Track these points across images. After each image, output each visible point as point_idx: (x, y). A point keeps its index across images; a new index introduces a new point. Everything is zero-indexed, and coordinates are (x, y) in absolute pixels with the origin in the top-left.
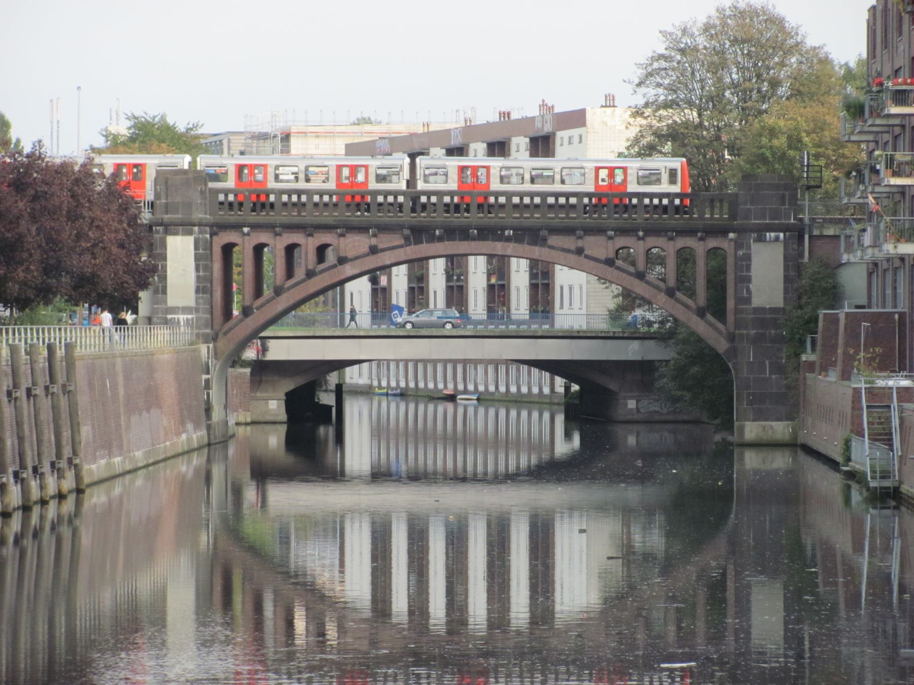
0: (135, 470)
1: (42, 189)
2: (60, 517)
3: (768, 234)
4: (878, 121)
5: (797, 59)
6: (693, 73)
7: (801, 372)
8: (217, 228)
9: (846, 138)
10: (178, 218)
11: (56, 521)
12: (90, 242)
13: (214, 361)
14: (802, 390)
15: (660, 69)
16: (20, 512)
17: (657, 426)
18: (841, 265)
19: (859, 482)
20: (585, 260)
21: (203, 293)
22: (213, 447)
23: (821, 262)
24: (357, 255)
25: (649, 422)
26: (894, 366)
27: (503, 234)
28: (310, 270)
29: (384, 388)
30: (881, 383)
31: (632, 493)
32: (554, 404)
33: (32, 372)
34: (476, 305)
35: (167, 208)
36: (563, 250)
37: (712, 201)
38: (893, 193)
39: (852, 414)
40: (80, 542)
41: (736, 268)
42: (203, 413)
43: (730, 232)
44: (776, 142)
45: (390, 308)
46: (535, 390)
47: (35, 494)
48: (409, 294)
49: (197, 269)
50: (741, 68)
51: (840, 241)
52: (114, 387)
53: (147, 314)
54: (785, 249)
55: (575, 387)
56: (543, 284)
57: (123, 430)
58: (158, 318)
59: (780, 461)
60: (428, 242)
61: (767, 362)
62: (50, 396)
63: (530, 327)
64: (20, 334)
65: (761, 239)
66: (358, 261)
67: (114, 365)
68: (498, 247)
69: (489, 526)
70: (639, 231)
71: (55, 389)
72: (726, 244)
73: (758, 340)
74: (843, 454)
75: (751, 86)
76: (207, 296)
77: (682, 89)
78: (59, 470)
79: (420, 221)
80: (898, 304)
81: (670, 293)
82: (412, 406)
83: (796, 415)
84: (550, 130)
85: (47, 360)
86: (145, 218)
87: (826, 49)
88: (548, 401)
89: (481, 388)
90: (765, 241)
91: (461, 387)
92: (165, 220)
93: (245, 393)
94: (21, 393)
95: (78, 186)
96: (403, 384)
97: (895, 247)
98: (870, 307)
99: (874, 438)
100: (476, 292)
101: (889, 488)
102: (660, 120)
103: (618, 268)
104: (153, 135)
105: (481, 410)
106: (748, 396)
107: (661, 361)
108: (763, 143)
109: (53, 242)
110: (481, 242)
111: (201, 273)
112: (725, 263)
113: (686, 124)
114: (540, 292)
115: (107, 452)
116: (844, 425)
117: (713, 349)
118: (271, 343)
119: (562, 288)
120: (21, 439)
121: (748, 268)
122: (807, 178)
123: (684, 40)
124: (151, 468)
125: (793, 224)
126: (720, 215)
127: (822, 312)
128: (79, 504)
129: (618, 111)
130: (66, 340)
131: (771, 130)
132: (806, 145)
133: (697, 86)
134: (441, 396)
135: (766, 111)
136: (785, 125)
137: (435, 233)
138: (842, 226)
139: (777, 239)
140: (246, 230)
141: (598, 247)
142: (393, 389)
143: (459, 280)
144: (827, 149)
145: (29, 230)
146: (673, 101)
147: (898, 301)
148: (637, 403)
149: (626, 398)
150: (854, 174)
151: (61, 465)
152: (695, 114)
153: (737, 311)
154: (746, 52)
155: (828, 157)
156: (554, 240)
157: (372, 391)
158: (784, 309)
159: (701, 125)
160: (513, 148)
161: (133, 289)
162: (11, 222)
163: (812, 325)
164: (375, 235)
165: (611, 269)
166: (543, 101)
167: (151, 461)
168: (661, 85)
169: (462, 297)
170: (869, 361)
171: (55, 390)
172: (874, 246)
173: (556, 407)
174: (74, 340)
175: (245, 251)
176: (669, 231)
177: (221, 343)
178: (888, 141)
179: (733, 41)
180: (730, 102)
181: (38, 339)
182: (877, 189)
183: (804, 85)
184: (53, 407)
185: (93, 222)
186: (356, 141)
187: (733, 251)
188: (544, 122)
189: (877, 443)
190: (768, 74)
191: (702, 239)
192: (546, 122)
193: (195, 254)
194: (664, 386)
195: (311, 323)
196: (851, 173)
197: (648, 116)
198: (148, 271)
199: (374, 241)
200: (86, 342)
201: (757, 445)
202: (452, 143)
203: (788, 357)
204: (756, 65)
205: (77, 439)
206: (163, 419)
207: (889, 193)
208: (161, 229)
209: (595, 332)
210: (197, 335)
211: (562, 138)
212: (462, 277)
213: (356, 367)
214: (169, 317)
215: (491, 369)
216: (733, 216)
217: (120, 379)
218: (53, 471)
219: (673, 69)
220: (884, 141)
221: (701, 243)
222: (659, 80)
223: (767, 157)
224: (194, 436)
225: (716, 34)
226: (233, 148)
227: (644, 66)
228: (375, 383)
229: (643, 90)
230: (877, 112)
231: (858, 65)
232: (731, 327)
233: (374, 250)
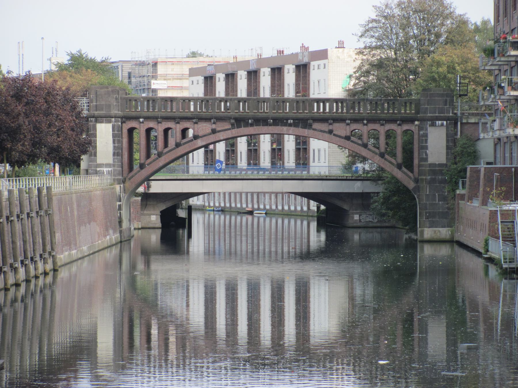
0: (83, 258)
1: (31, 99)
2: (44, 285)
3: (437, 122)
4: (503, 59)
5: (450, 22)
6: (391, 30)
7: (456, 200)
8: (125, 119)
9: (483, 68)
10: (103, 113)
11: (43, 287)
12: (56, 128)
13: (124, 194)
14: (457, 210)
15: (373, 27)
16: (25, 283)
17: (371, 230)
18: (479, 139)
19: (496, 264)
20: (334, 137)
21: (117, 156)
22: (123, 243)
23: (467, 137)
24: (204, 134)
25: (366, 227)
26: (512, 198)
28: (178, 143)
29: (212, 207)
30: (505, 208)
31: (357, 268)
32: (310, 216)
33: (30, 203)
34: (264, 160)
35: (97, 108)
36: (321, 131)
37: (406, 103)
38: (510, 99)
39: (489, 225)
40: (55, 299)
41: (419, 141)
42: (118, 223)
44: (440, 70)
45: (215, 161)
46: (299, 208)
47: (32, 273)
48: (226, 154)
49: (114, 142)
50: (419, 27)
52: (72, 211)
53: (86, 168)
54: (447, 130)
55: (323, 207)
56: (303, 148)
57: (77, 235)
58: (92, 170)
59: (444, 251)
60: (244, 127)
61: (437, 194)
62: (39, 217)
63: (295, 173)
64: (23, 182)
65: (433, 125)
66: (205, 137)
67: (72, 198)
68: (251, 130)
69: (272, 285)
70: (364, 120)
71: (42, 213)
72: (413, 127)
73: (432, 182)
74: (484, 247)
75: (425, 37)
76: (119, 157)
77: (385, 39)
78: (44, 258)
79: (240, 115)
80: (513, 162)
81: (382, 155)
82: (228, 217)
83: (453, 224)
84: (307, 61)
85: (37, 197)
86: (85, 114)
87: (467, 16)
88: (306, 214)
89: (268, 207)
90: (436, 126)
91: (256, 206)
92: (96, 115)
93: (138, 212)
94: (25, 216)
95: (49, 96)
96: (222, 205)
97: (514, 131)
98: (495, 164)
99: (505, 239)
100: (264, 152)
101: (514, 268)
102: (373, 57)
103: (352, 142)
104: (83, 65)
105: (268, 220)
106: (426, 213)
107: (374, 193)
108: (433, 70)
109: (37, 129)
110: (274, 127)
111: (116, 145)
112: (413, 138)
113: (388, 59)
114: (301, 153)
115: (68, 247)
116: (484, 231)
117: (405, 186)
118: (153, 183)
119: (314, 150)
120: (25, 242)
121: (426, 141)
122: (460, 90)
123: (386, 11)
124: (91, 256)
125: (451, 116)
126: (410, 111)
127: (469, 167)
128: (55, 277)
129: (346, 50)
130: (46, 185)
131: (438, 63)
132: (458, 71)
133: (394, 37)
134: (244, 211)
135: (433, 52)
136: (446, 60)
137: (248, 122)
138: (479, 117)
139: (442, 125)
140: (141, 120)
141: (341, 129)
142: (217, 207)
143: (254, 146)
144: (469, 73)
145: (24, 122)
146: (380, 45)
147: (513, 161)
148: (359, 217)
149: (353, 214)
150: (488, 88)
151: (46, 256)
152: (393, 53)
153: (419, 166)
154: (422, 17)
155: (470, 78)
156: (316, 126)
157: (204, 209)
158: (446, 165)
159: (396, 59)
161: (79, 154)
162: (14, 118)
163: (462, 174)
164: (214, 123)
165: (347, 142)
166: (303, 44)
167: (91, 252)
168: (374, 36)
169: (257, 155)
170: (498, 195)
171: (42, 214)
172: (500, 130)
173: (311, 218)
174: (50, 185)
176: (381, 120)
177: (127, 184)
178: (507, 70)
179: (415, 11)
180: (413, 46)
181: (32, 184)
182: (502, 97)
183: (455, 36)
184: (41, 223)
185: (57, 117)
186: (194, 67)
187: (417, 131)
188: (303, 56)
189: (507, 243)
190: (434, 30)
191: (399, 125)
192: (305, 56)
193: (113, 133)
194: (376, 207)
195: (173, 171)
196: (486, 88)
197: (367, 54)
198: (87, 144)
199: (214, 126)
200: (57, 186)
201: (430, 242)
202: (251, 68)
203: (449, 192)
204: (427, 25)
205: (54, 241)
206: (96, 228)
207: (508, 99)
208: (93, 119)
209: (337, 176)
210: (114, 180)
211: (314, 66)
212: (257, 144)
213: (201, 197)
214: (98, 169)
215: (273, 196)
216: (418, 112)
217: (75, 206)
218: (41, 260)
219: (381, 28)
220: (504, 70)
221: (400, 127)
222: (372, 33)
223: (436, 78)
224: (113, 237)
225: (404, 7)
226: (124, 70)
227: (364, 26)
228: (207, 204)
229: (363, 39)
230: (503, 54)
231: (482, 24)
232: (417, 176)
233: (214, 132)
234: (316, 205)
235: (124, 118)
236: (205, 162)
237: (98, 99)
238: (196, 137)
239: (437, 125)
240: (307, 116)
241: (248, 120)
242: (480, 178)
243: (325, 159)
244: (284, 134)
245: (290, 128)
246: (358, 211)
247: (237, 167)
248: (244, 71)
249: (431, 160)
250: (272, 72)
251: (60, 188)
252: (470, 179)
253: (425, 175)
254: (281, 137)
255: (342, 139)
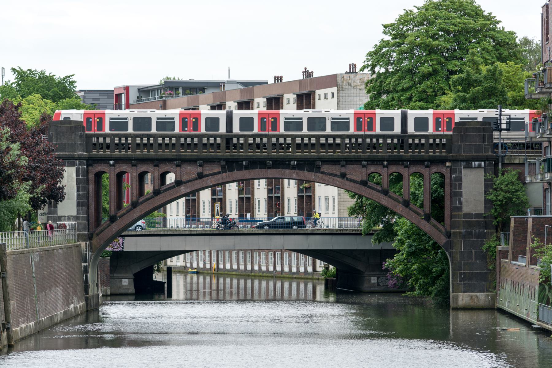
3: (473, 163)
13: (90, 253)
27: (290, 164)
28: (157, 190)
36: (331, 175)
43: (447, 161)
46: (302, 270)
48: (239, 203)
49: (78, 190)
51: (525, 167)
65: (468, 166)
70: (384, 161)
106: (461, 274)
110: (274, 170)
137: (242, 163)
139: (480, 166)
140: (111, 162)
153: (452, 217)
156: (326, 168)
157: (186, 271)
160: (285, 101)
166: (306, 69)
175: (111, 177)
176: (405, 161)
177: (95, 241)
187: (449, 174)
191: (427, 166)
193: (77, 179)
199: (200, 170)
201: (465, 309)
211: (319, 95)
213: (181, 256)
221: (428, 169)
224: (78, 306)
228: (189, 265)
232: (448, 228)
233: (201, 176)
234: (323, 265)
235: (91, 160)
236: (186, 214)
237: (59, 137)
238: (178, 183)
239: (473, 166)
240: (314, 156)
241: (242, 162)
242: (527, 231)
243: (334, 210)
244: (283, 178)
245: (293, 171)
246: (376, 273)
247: (199, 220)
248: (234, 102)
249: (466, 209)
250: (268, 103)
251: (15, 246)
252: (514, 232)
253: (458, 228)
254: (279, 182)
255: (358, 185)
